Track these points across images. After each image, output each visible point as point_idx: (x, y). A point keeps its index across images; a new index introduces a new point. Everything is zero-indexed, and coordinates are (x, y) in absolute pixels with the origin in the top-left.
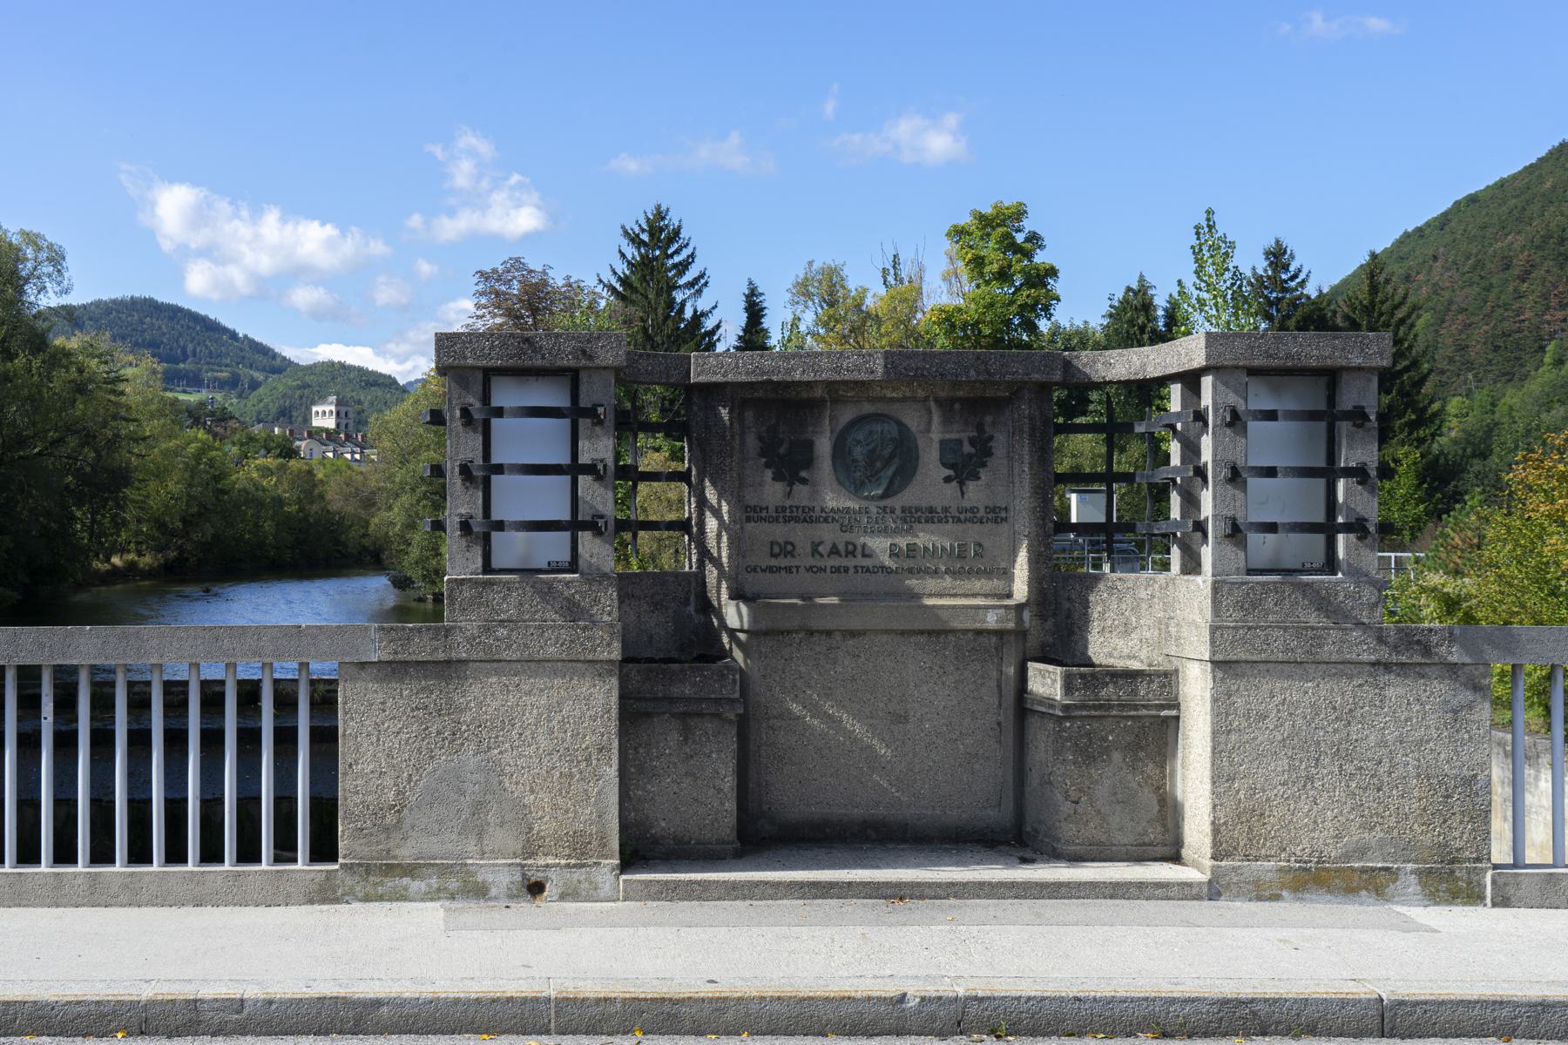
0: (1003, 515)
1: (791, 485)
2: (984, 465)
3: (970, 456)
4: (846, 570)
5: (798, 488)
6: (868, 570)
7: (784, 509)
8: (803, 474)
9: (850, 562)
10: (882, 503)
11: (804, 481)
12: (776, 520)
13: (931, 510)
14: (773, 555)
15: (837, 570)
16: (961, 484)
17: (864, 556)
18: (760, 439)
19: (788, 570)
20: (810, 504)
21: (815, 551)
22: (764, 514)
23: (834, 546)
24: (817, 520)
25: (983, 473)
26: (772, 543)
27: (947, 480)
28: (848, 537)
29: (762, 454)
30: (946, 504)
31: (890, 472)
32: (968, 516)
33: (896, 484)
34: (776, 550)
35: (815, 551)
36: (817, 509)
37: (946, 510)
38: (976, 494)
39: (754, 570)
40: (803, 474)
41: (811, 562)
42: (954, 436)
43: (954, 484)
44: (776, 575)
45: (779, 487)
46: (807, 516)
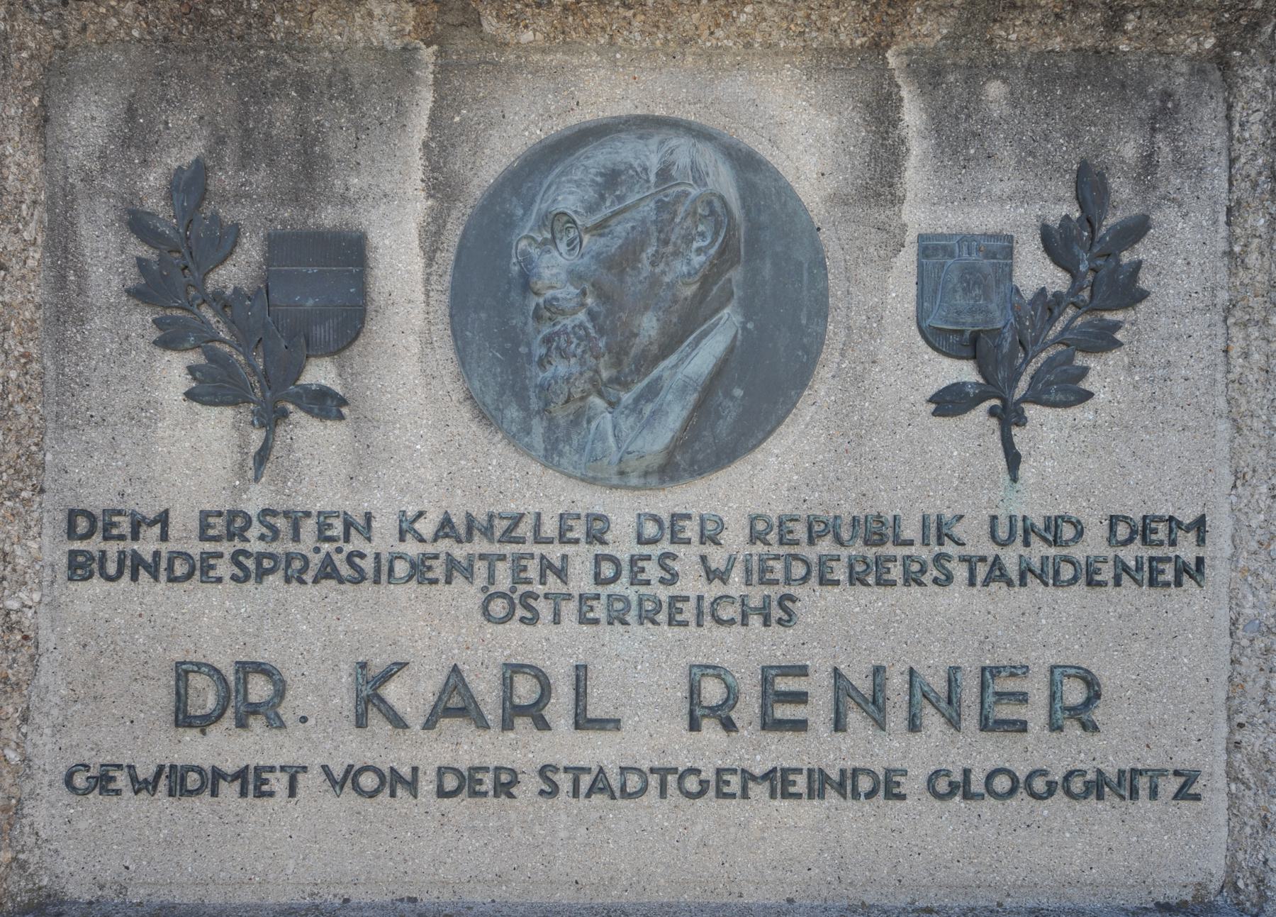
0: (1187, 550)
1: (271, 418)
2: (1103, 340)
3: (1048, 305)
4: (506, 786)
5: (307, 433)
6: (600, 785)
7: (236, 525)
8: (321, 373)
9: (522, 749)
10: (666, 501)
11: (326, 404)
12: (203, 569)
13: (877, 531)
14: (183, 718)
15: (465, 783)
16: (1008, 417)
17: (582, 722)
18: (138, 223)
19: (252, 781)
20: (355, 507)
21: (370, 699)
22: (147, 545)
23: (455, 679)
24: (383, 572)
25: (1102, 373)
26: (182, 672)
27: (949, 402)
28: (516, 640)
29: (149, 289)
30: (940, 505)
31: (703, 357)
32: (1040, 552)
33: (731, 412)
34: (205, 697)
35: (370, 699)
36: (385, 526)
37: (940, 530)
38: (1068, 460)
39: (103, 782)
40: (321, 373)
41: (352, 748)
42: (983, 219)
43: (979, 418)
44: (202, 803)
45: (220, 430)
46: (333, 555)
